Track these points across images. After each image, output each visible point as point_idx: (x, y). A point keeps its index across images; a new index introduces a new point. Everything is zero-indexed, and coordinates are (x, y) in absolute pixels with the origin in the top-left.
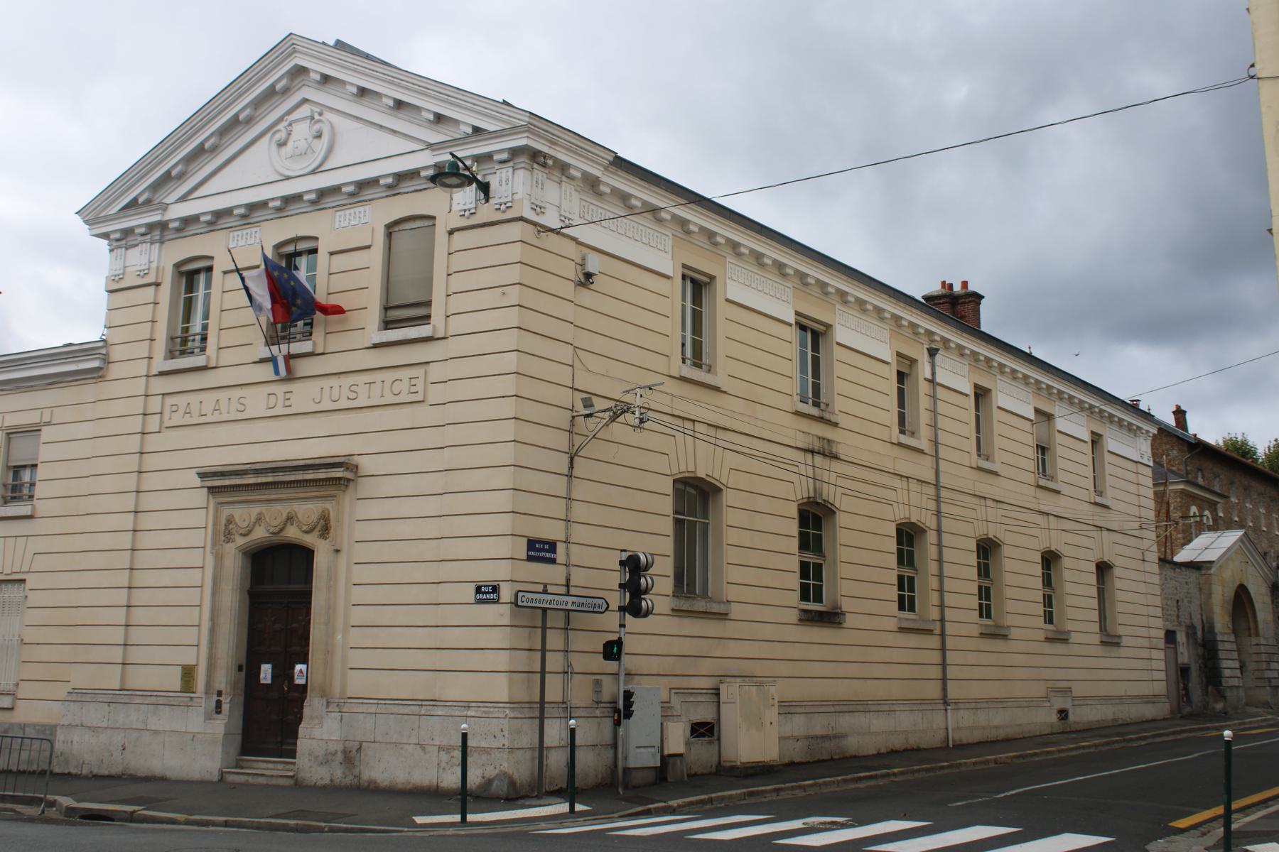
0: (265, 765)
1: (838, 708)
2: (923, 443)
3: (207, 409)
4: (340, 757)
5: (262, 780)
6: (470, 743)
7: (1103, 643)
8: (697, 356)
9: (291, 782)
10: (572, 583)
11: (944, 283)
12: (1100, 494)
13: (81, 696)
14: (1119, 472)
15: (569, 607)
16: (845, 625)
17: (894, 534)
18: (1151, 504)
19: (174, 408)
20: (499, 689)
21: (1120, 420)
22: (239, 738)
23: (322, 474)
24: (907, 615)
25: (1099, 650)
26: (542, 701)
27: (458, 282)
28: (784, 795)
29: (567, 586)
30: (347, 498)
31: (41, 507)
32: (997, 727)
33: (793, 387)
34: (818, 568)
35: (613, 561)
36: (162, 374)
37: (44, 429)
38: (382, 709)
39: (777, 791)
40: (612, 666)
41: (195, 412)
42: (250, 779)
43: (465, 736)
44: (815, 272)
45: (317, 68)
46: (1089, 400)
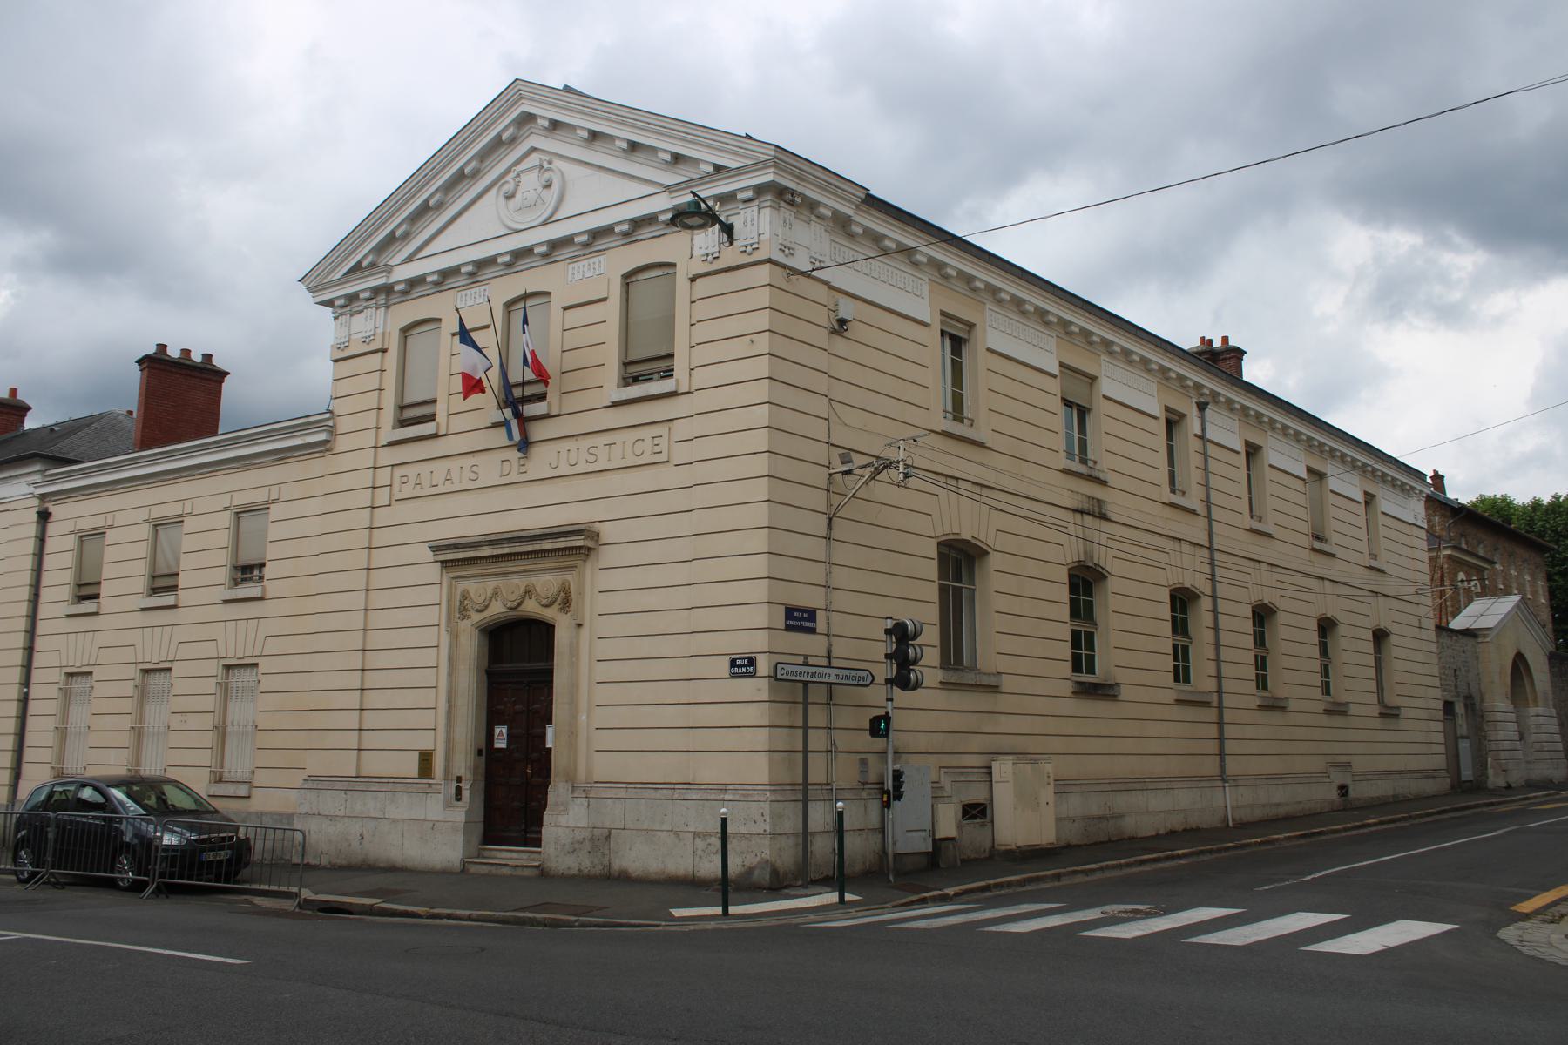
0: (508, 855)
1: (1115, 787)
2: (1194, 501)
3: (439, 478)
5: (506, 871)
7: (1382, 715)
8: (957, 410)
9: (536, 872)
10: (834, 654)
11: (1203, 339)
12: (1375, 557)
13: (317, 783)
14: (1393, 535)
15: (832, 680)
16: (1121, 697)
17: (1168, 600)
18: (1426, 568)
20: (759, 770)
21: (1394, 479)
22: (481, 826)
24: (1183, 686)
25: (1378, 723)
27: (702, 332)
28: (1065, 881)
29: (829, 657)
30: (588, 568)
31: (272, 588)
32: (1278, 805)
33: (1059, 443)
34: (1090, 637)
35: (878, 630)
36: (391, 444)
38: (632, 793)
39: (1058, 877)
40: (879, 744)
41: (426, 484)
42: (493, 869)
43: (724, 821)
44: (1079, 320)
45: (545, 113)
46: (1363, 458)
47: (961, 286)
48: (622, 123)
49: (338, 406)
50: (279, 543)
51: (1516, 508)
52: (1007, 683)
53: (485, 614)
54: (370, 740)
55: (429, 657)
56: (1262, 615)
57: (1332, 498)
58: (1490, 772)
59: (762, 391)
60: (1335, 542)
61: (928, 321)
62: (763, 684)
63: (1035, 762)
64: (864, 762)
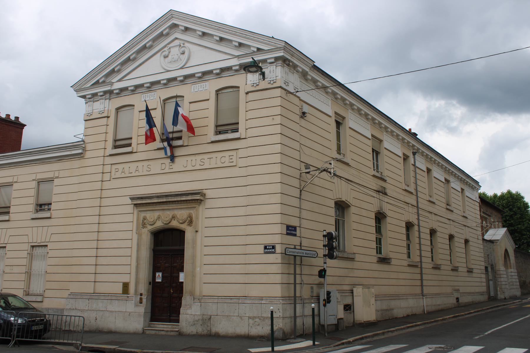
2: (412, 189)
3: (133, 170)
4: (201, 322)
5: (163, 333)
6: (274, 316)
7: (468, 271)
9: (177, 333)
10: (302, 245)
13: (74, 296)
14: (470, 204)
16: (392, 263)
19: (117, 170)
20: (277, 291)
22: (150, 314)
23: (189, 198)
26: (295, 296)
27: (251, 114)
29: (301, 246)
30: (201, 208)
31: (54, 214)
32: (439, 305)
36: (111, 155)
37: (55, 180)
42: (157, 332)
43: (272, 312)
45: (183, 24)
47: (340, 102)
48: (218, 30)
49: (87, 140)
50: (58, 194)
51: (488, 197)
52: (357, 258)
53: (154, 226)
54: (99, 278)
55: (128, 244)
56: (433, 232)
57: (452, 190)
58: (499, 293)
59: (277, 139)
60: (453, 207)
61: (331, 115)
62: (279, 256)
63: (369, 288)
64: (312, 288)
